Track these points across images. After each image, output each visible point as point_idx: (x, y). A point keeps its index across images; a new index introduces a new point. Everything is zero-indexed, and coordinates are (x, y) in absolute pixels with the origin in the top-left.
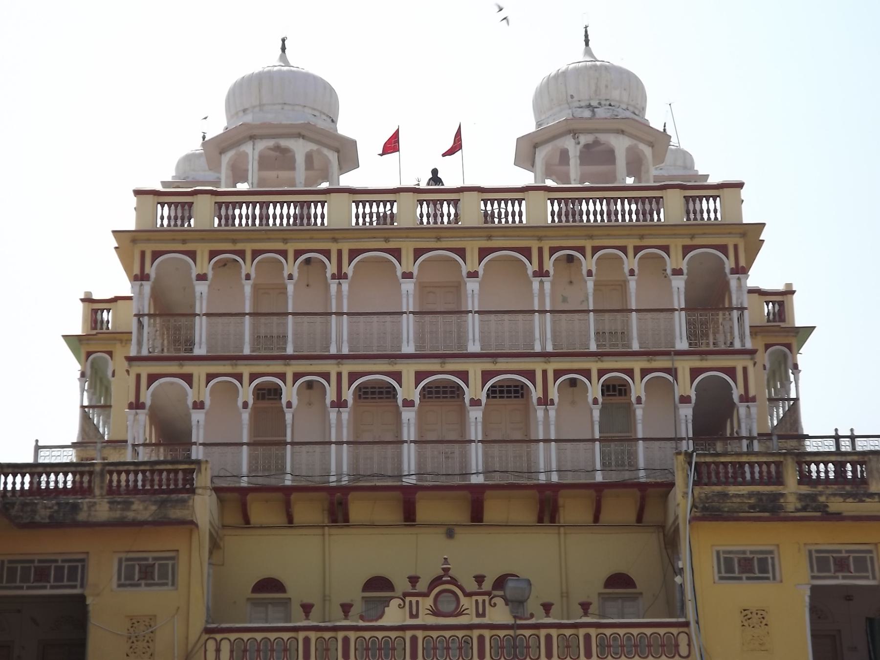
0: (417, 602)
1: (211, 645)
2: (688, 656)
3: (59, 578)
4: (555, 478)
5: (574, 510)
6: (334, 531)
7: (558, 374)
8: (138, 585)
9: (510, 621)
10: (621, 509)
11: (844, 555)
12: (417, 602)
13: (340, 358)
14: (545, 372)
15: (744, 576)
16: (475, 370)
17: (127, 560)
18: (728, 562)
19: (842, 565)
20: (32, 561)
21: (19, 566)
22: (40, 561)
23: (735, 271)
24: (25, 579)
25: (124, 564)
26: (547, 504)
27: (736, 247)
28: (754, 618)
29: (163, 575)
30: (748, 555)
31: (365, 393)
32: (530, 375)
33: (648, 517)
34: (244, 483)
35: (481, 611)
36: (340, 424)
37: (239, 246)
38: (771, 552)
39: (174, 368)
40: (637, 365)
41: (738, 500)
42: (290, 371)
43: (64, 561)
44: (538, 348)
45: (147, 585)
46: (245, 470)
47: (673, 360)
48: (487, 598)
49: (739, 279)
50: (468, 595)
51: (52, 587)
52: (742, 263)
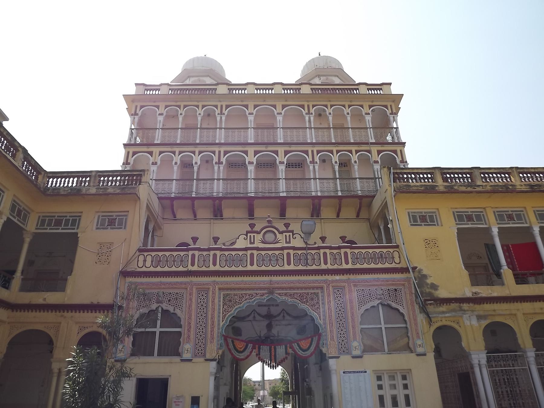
0: (254, 236)
1: (141, 258)
2: (399, 263)
3: (66, 224)
4: (319, 194)
5: (327, 212)
6: (216, 221)
7: (318, 152)
8: (107, 228)
9: (304, 246)
10: (348, 212)
11: (470, 213)
12: (254, 236)
13: (220, 144)
14: (312, 151)
15: (423, 224)
16: (281, 150)
17: (103, 216)
18: (414, 217)
19: (470, 218)
20: (54, 216)
21: (47, 219)
22: (58, 216)
23: (392, 114)
24: (49, 224)
25: (101, 218)
26: (315, 207)
27: (391, 106)
28: (430, 243)
29: (120, 224)
30: (424, 214)
31: (232, 165)
32: (306, 152)
33: (362, 215)
34: (173, 195)
35: (288, 241)
36: (219, 171)
37: (178, 104)
38: (434, 212)
39: (145, 149)
40: (354, 148)
41: (416, 188)
42: (197, 151)
43: (70, 217)
44: (309, 141)
45: (111, 228)
46: (173, 190)
47: (370, 147)
48: (291, 234)
49: (394, 117)
50: (281, 233)
51: (62, 229)
52: (394, 111)
